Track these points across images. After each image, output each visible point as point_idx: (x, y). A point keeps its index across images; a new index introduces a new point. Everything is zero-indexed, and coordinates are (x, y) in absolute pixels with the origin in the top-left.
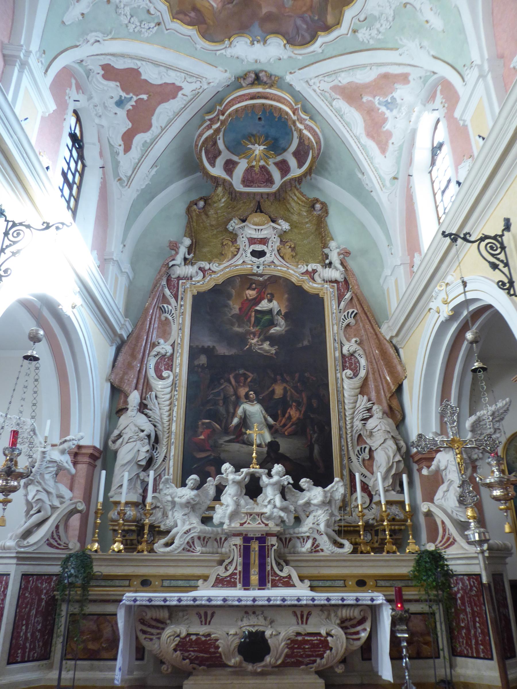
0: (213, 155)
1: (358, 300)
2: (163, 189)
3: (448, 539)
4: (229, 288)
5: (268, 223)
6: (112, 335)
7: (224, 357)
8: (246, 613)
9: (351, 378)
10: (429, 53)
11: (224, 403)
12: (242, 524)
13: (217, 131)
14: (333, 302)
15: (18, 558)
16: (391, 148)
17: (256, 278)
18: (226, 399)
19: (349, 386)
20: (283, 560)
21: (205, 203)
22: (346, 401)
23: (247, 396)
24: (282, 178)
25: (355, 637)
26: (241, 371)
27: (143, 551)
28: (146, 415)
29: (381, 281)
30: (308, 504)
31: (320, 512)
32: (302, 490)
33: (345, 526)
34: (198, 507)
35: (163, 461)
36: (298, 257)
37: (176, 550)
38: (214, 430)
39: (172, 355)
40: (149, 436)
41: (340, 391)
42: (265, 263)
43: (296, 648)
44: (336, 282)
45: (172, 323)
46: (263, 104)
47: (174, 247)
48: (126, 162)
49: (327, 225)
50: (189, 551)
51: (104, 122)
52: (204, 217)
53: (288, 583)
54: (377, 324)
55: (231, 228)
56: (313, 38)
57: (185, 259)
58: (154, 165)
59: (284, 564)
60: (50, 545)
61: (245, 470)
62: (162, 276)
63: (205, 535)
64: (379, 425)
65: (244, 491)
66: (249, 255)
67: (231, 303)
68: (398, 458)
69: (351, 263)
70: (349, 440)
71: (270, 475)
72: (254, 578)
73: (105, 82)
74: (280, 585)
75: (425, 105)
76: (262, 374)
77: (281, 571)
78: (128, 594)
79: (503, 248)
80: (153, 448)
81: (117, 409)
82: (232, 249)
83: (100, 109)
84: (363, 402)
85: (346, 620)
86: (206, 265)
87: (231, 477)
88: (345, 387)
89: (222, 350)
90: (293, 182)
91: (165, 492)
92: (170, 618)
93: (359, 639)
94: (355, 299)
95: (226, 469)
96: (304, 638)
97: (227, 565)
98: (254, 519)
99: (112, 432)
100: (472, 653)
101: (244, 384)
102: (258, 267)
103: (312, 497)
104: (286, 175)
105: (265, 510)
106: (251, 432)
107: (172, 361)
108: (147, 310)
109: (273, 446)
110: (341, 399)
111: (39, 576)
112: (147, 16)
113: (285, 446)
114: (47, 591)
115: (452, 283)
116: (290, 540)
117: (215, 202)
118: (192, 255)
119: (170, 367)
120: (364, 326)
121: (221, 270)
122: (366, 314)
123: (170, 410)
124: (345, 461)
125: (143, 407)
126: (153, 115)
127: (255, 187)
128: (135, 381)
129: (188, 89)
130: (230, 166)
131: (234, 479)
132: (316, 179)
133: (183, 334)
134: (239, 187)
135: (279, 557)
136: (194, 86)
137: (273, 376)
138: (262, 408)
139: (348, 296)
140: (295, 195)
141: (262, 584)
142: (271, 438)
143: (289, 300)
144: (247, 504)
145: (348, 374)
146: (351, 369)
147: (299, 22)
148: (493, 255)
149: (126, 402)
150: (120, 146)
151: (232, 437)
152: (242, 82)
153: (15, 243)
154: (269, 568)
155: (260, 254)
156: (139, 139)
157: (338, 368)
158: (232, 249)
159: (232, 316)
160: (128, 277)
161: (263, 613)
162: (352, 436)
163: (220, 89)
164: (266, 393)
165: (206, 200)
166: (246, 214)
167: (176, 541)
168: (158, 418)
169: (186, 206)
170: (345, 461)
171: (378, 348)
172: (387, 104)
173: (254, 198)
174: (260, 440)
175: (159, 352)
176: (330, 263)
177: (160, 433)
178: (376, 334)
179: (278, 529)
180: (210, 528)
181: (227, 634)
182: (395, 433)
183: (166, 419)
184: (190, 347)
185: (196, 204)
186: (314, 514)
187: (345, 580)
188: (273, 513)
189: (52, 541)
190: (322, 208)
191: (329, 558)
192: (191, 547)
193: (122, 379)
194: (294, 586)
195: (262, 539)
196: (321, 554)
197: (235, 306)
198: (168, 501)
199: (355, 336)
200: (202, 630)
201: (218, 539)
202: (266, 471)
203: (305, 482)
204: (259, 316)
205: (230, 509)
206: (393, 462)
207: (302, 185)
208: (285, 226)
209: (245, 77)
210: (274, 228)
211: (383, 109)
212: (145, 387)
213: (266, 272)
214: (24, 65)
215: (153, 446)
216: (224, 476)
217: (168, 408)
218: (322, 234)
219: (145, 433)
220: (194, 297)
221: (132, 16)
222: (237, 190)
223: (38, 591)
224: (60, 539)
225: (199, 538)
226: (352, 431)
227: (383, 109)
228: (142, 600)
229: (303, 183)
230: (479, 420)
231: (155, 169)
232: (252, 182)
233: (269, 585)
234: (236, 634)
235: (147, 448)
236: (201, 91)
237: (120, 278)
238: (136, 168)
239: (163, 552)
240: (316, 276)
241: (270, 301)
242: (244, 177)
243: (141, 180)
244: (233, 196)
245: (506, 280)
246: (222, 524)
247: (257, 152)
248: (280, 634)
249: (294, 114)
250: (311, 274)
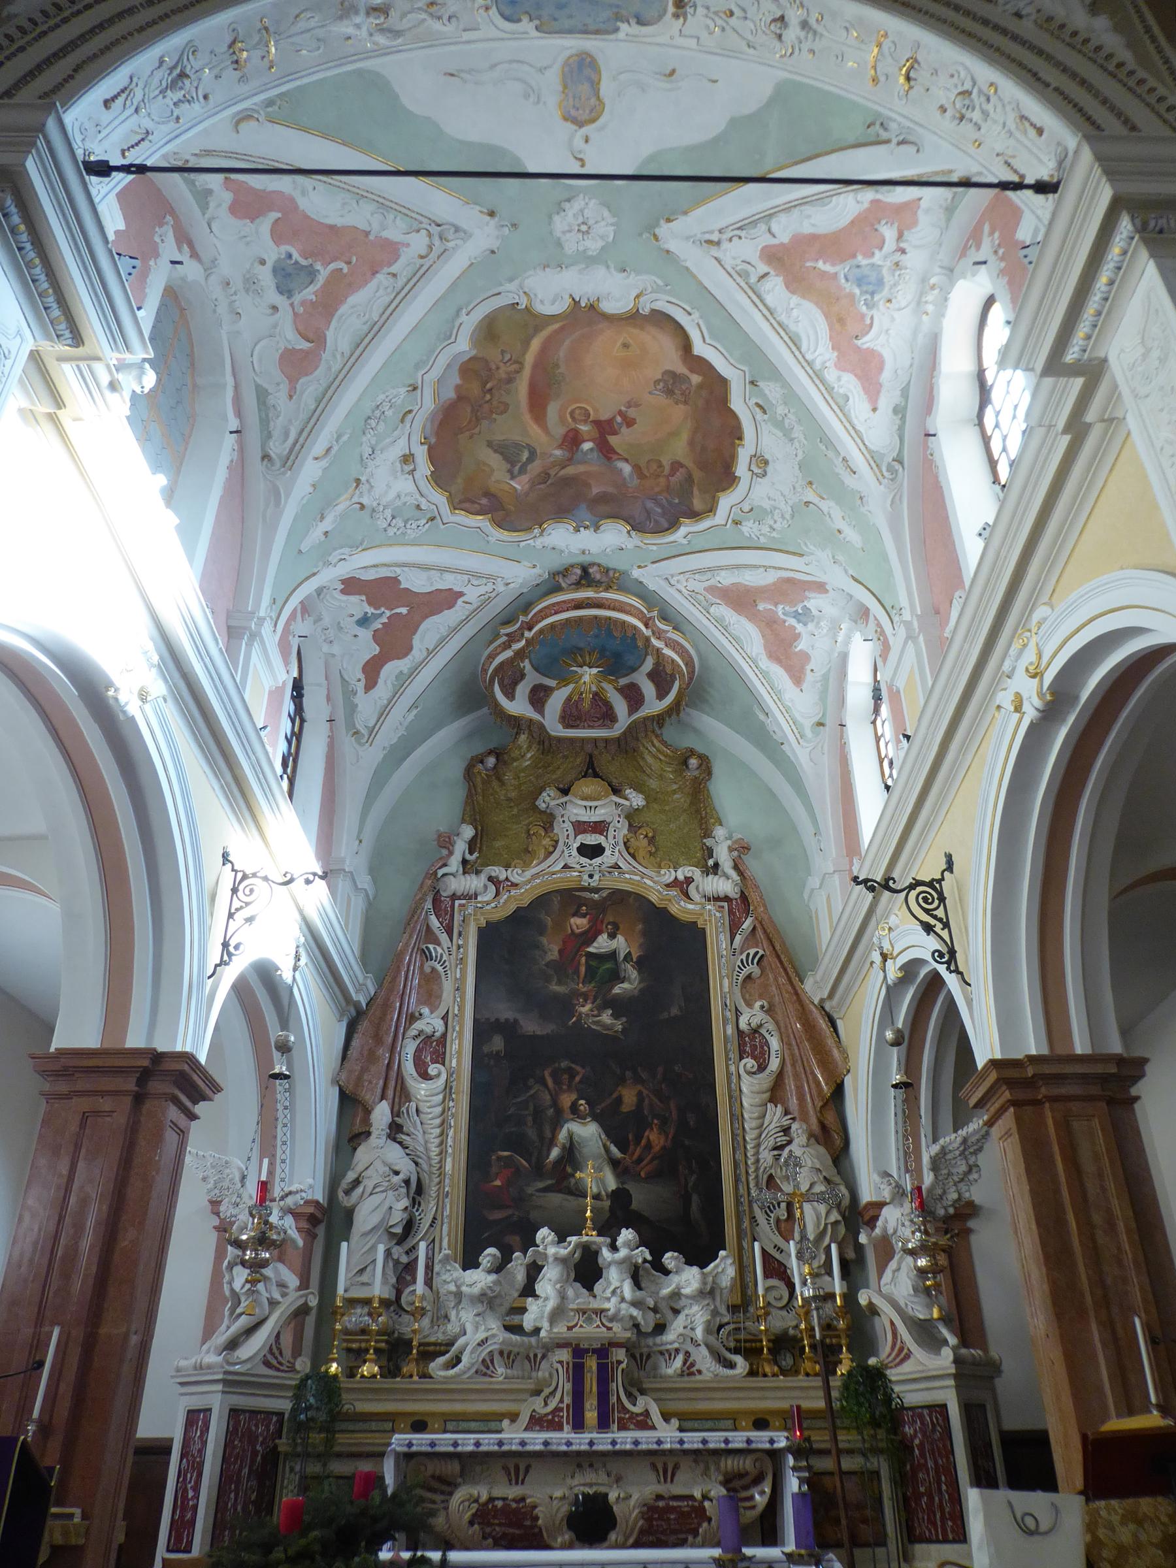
0: (510, 678)
1: (765, 932)
3: (901, 1349)
4: (543, 916)
5: (607, 796)
6: (344, 1004)
7: (534, 1037)
8: (579, 1466)
9: (754, 1073)
10: (846, 571)
11: (534, 1121)
12: (570, 1328)
13: (520, 655)
14: (722, 937)
15: (225, 1382)
16: (809, 677)
17: (587, 895)
18: (538, 1114)
19: (752, 1088)
20: (635, 1388)
21: (497, 760)
22: (746, 1116)
23: (574, 1108)
24: (631, 713)
25: (748, 1504)
26: (564, 1064)
27: (411, 1376)
28: (400, 1143)
29: (806, 896)
30: (676, 1295)
31: (695, 1308)
32: (666, 1272)
33: (746, 1341)
34: (498, 1301)
35: (431, 1226)
36: (660, 853)
37: (465, 1373)
38: (518, 1170)
39: (444, 1035)
41: (735, 1097)
42: (603, 867)
43: (656, 1519)
44: (727, 899)
45: (443, 977)
46: (596, 617)
47: (446, 842)
48: (367, 705)
49: (709, 796)
50: (485, 1375)
51: (336, 649)
52: (495, 784)
53: (643, 1422)
54: (798, 975)
55: (543, 806)
56: (673, 525)
57: (464, 862)
58: (414, 705)
59: (637, 1393)
60: (267, 1364)
61: (573, 1239)
62: (425, 895)
63: (511, 1348)
64: (808, 1158)
65: (573, 1275)
66: (575, 853)
67: (544, 940)
68: (835, 1216)
69: (753, 865)
70: (752, 1185)
71: (614, 1248)
72: (591, 1416)
73: (344, 598)
74: (632, 1426)
75: (856, 622)
76: (600, 1070)
77: (634, 1405)
78: (396, 1436)
79: (942, 899)
80: (414, 1202)
81: (350, 1134)
82: (544, 842)
83: (331, 633)
84: (775, 1116)
85: (734, 1477)
86: (500, 872)
87: (552, 1250)
88: (744, 1089)
89: (531, 1026)
90: (648, 723)
91: (444, 1277)
92: (462, 1474)
93: (753, 1507)
94: (760, 931)
95: (544, 1238)
96: (668, 1505)
97: (548, 1397)
98: (589, 1320)
99: (344, 1176)
100: (937, 1535)
101: (569, 1086)
102: (591, 876)
103: (682, 1283)
104: (637, 710)
105: (606, 1305)
106: (582, 1175)
107: (444, 1046)
108: (399, 957)
109: (620, 1197)
110: (738, 1112)
111: (254, 1413)
112: (418, 513)
113: (641, 1197)
114: (265, 1439)
115: (897, 927)
116: (649, 1356)
117: (515, 760)
118: (476, 855)
119: (440, 1058)
120: (776, 979)
121: (528, 880)
122: (778, 957)
123: (442, 1134)
124: (746, 1224)
125: (395, 1130)
126: (414, 633)
127: (584, 728)
128: (381, 1082)
129: (473, 594)
130: (539, 697)
131: (557, 1253)
132: (688, 714)
133: (463, 997)
134: (556, 729)
135: (632, 1385)
136: (482, 590)
137: (618, 1071)
138: (600, 1130)
139: (747, 924)
140: (654, 746)
141: (603, 1424)
142: (617, 1183)
143: (644, 933)
144: (577, 1296)
145: (749, 1066)
146: (754, 1057)
147: (650, 505)
148: (927, 911)
149: (366, 1121)
150: (359, 680)
151: (550, 1182)
152: (561, 580)
153: (247, 904)
154: (613, 1399)
155: (592, 851)
156: (390, 670)
157: (731, 1055)
158: (544, 842)
159: (547, 965)
160: (367, 895)
161: (605, 1466)
162: (757, 1177)
163: (525, 590)
164: (608, 1101)
165: (498, 753)
166: (569, 778)
167: (465, 1359)
168: (421, 1149)
169: (463, 765)
170: (746, 1224)
171: (800, 1019)
172: (796, 615)
173: (582, 748)
174: (598, 1187)
175: (422, 1031)
176: (716, 865)
177: (425, 1178)
178: (797, 994)
179: (628, 1335)
180: (518, 1338)
181: (550, 1496)
182: (831, 1172)
183: (434, 1151)
184: (475, 1021)
185: (482, 762)
186: (686, 1311)
187: (735, 1420)
188: (619, 1310)
189: (269, 1357)
190: (701, 765)
191: (711, 1385)
192: (488, 1368)
193: (359, 1079)
194: (653, 1428)
195: (602, 1352)
196: (698, 1377)
198: (451, 1293)
199: (761, 997)
200: (513, 1492)
201: (532, 1356)
202: (608, 1240)
203: (672, 1257)
204: (593, 963)
205: (551, 1305)
206: (826, 1225)
207: (664, 730)
208: (636, 800)
209: (565, 572)
210: (617, 805)
211: (792, 621)
212: (398, 1094)
213: (606, 883)
214: (254, 636)
215: (414, 1199)
216: (541, 1249)
217: (438, 1131)
218: (701, 812)
219: (401, 1176)
220: (482, 932)
221: (394, 518)
222: (553, 734)
223: (252, 1438)
224: (281, 1353)
225: (501, 1353)
226: (757, 1169)
227: (792, 621)
228: (421, 1445)
229: (667, 724)
230: (943, 1151)
231: (415, 712)
232: (579, 718)
234: (564, 1498)
235: (405, 1202)
236: (493, 595)
237: (353, 899)
238: (383, 713)
239: (445, 1377)
240: (692, 890)
241: (612, 936)
242: (564, 711)
243: (389, 734)
244: (546, 744)
245: (944, 950)
246: (537, 1331)
247: (586, 678)
248: (630, 1497)
249: (647, 626)
250: (683, 887)
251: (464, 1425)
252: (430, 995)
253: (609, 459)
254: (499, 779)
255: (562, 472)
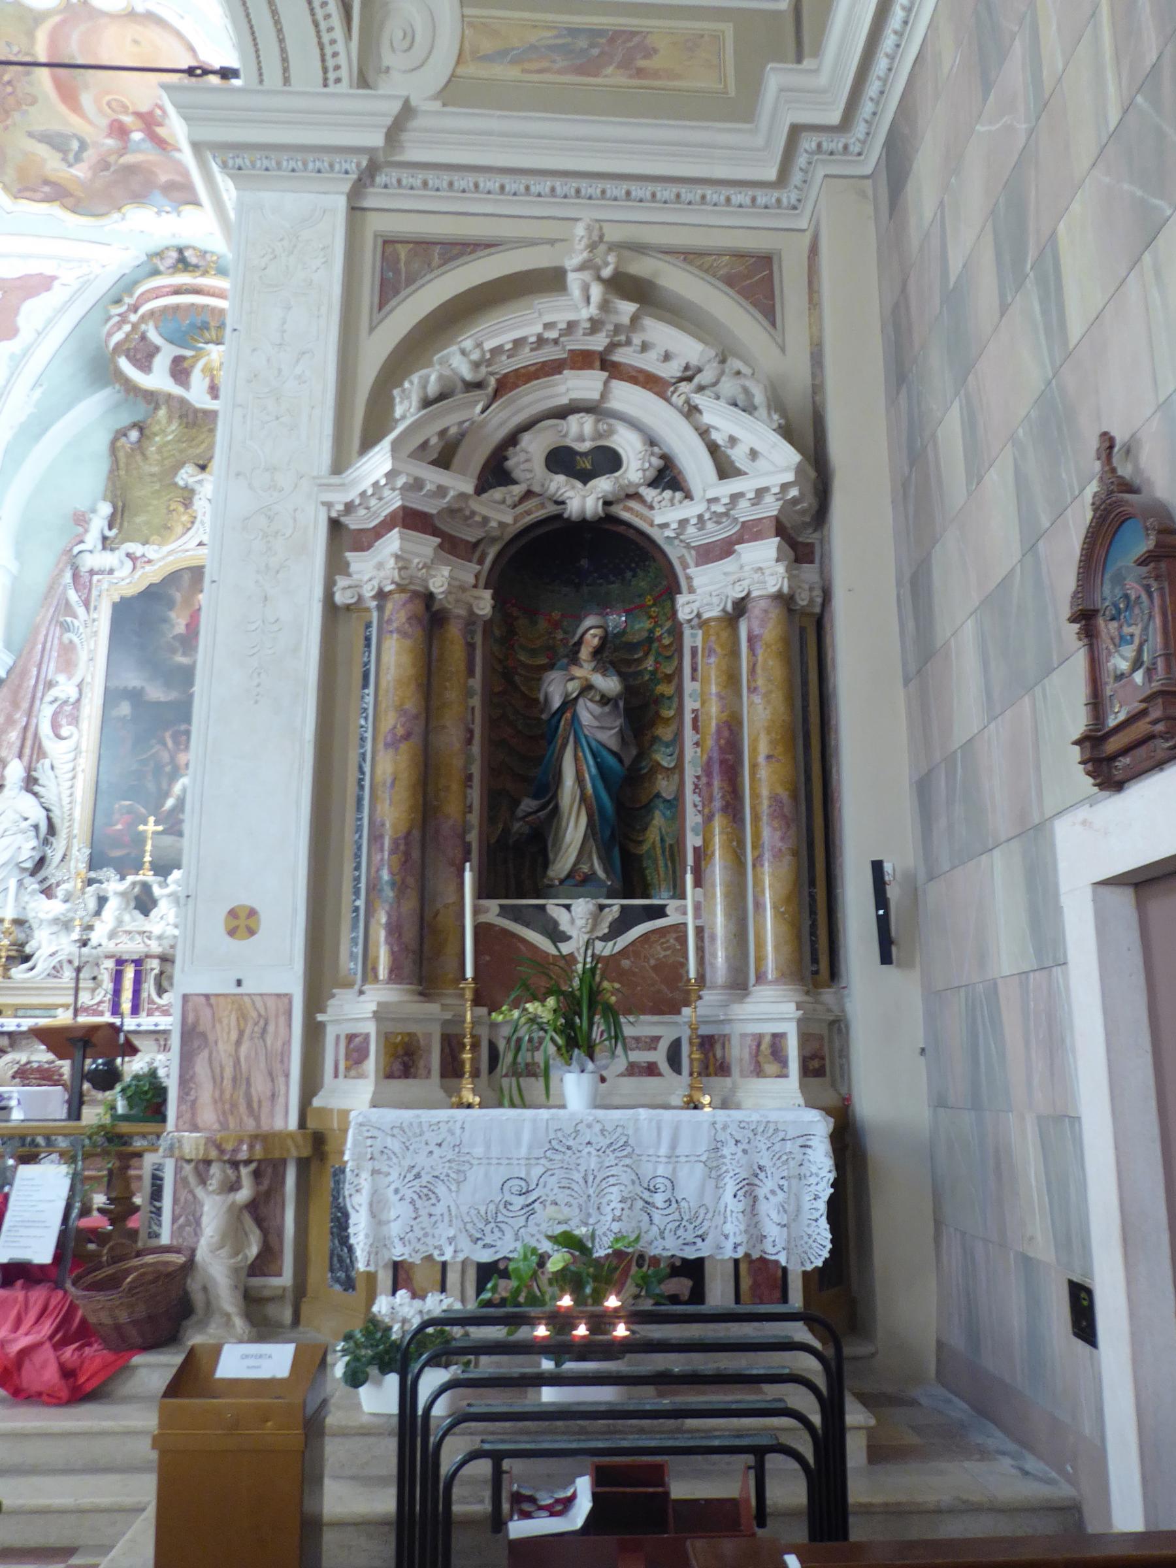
0: (144, 356)
2: (64, 414)
7: (158, 703)
39: (78, 700)
40: (36, 827)
45: (79, 646)
47: (81, 520)
52: (139, 458)
55: (181, 483)
57: (105, 539)
65: (133, 904)
67: (173, 615)
108: (35, 630)
118: (115, 531)
119: (75, 720)
121: (162, 558)
125: (30, 783)
154: (144, 995)
159: (174, 638)
163: (127, 271)
165: (140, 427)
177: (57, 821)
183: (66, 800)
185: (125, 435)
195: (138, 962)
197: (180, 620)
209: (160, 254)
212: (35, 752)
219: (29, 822)
222: (198, 405)
233: (144, 1014)
251: (30, 1013)
252: (68, 664)
253: (164, 149)
254: (143, 454)
255: (123, 160)
